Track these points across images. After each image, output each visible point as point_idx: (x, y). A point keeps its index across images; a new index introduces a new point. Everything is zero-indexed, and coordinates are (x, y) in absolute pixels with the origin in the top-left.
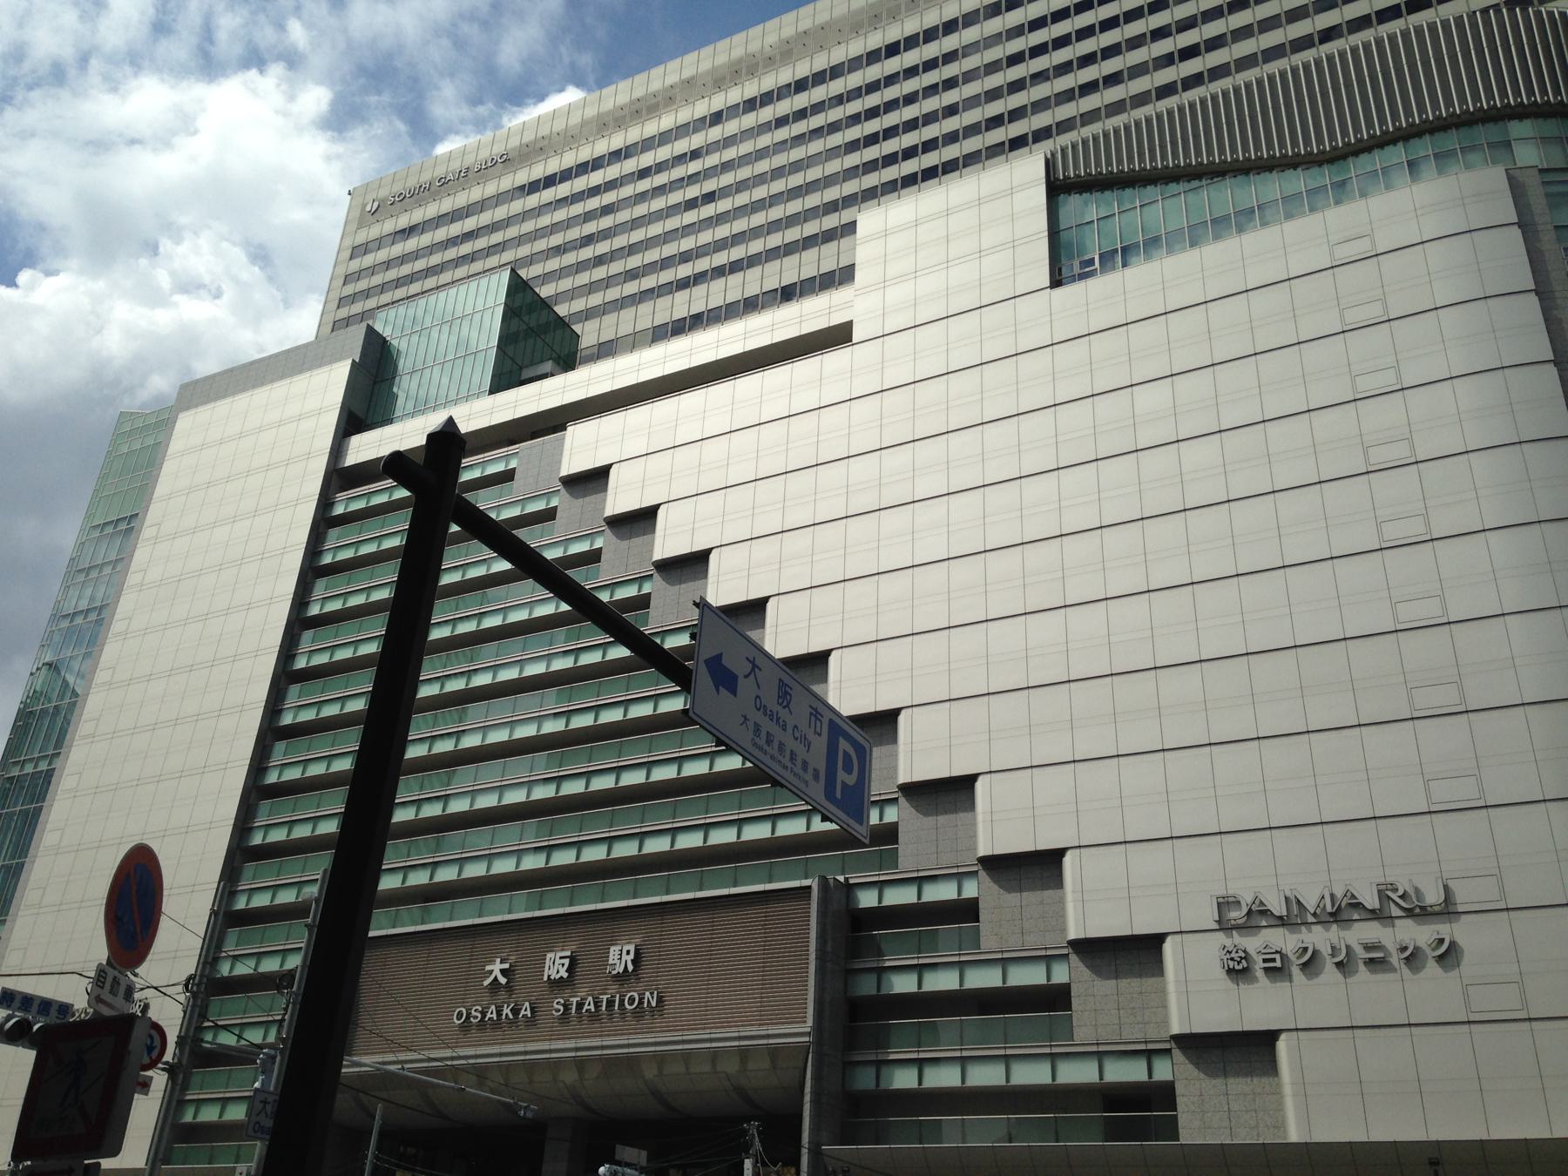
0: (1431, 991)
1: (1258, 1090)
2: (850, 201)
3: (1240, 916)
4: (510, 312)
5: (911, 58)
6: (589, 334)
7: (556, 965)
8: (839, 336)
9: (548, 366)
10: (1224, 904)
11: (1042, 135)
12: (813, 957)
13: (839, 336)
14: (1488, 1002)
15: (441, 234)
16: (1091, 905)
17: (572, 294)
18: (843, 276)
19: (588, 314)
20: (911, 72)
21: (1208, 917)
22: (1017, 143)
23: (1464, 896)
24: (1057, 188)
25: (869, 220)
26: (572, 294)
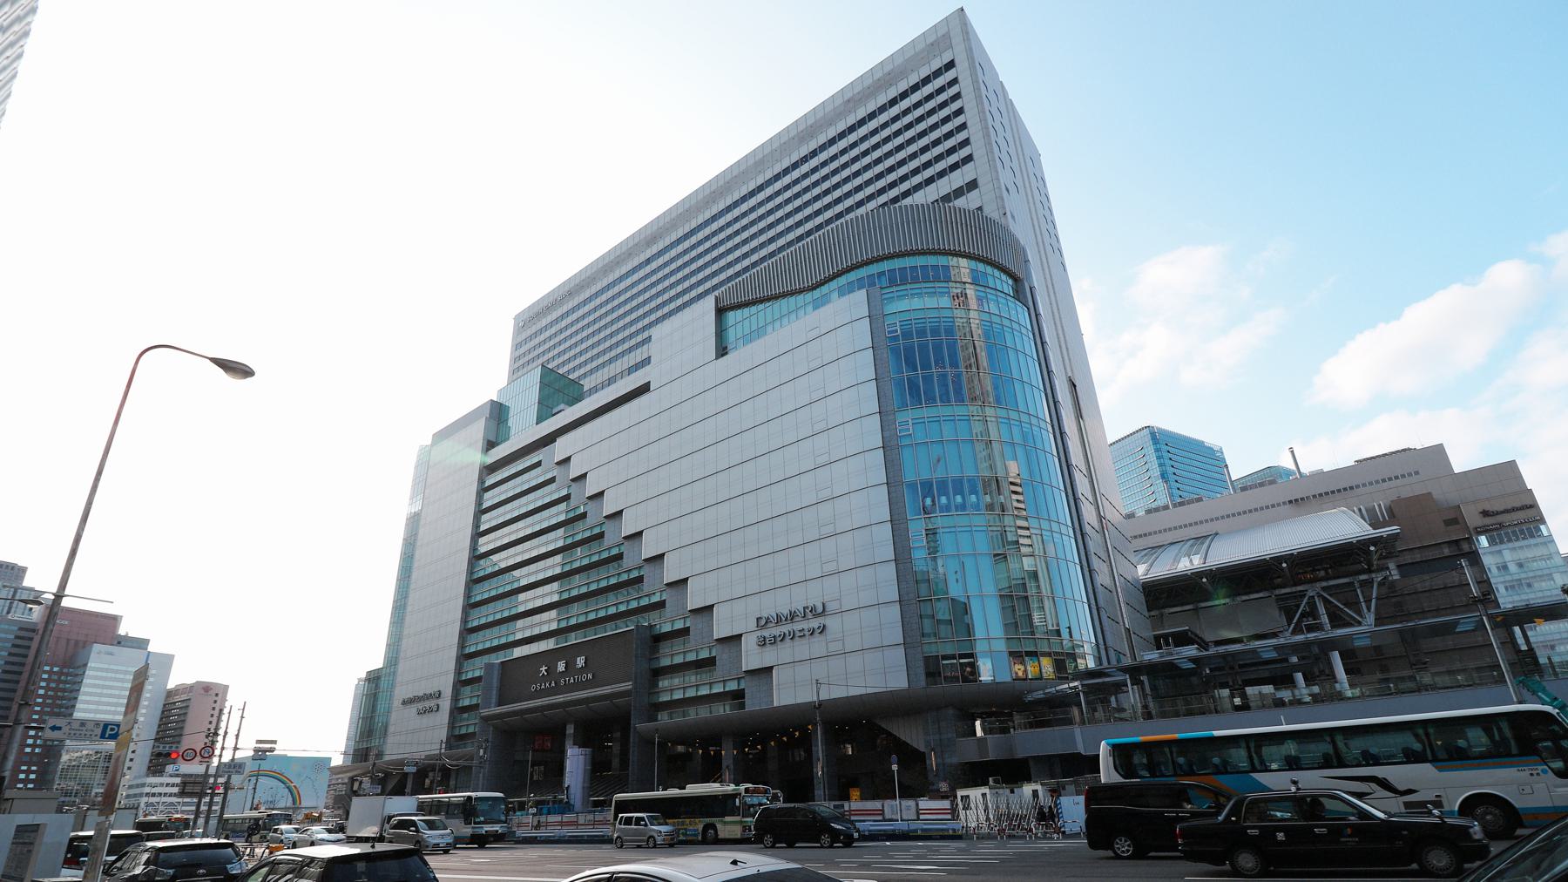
0: (817, 646)
1: (964, 435)
2: (650, 325)
3: (763, 623)
4: (544, 384)
5: (700, 235)
6: (587, 384)
7: (561, 667)
8: (644, 389)
9: (562, 406)
10: (758, 619)
11: (707, 292)
12: (607, 690)
13: (644, 389)
14: (834, 647)
15: (661, 261)
16: (722, 627)
17: (574, 370)
18: (647, 361)
19: (585, 375)
20: (824, 164)
21: (752, 625)
22: (700, 297)
23: (831, 607)
24: (721, 311)
25: (655, 332)
26: (574, 370)
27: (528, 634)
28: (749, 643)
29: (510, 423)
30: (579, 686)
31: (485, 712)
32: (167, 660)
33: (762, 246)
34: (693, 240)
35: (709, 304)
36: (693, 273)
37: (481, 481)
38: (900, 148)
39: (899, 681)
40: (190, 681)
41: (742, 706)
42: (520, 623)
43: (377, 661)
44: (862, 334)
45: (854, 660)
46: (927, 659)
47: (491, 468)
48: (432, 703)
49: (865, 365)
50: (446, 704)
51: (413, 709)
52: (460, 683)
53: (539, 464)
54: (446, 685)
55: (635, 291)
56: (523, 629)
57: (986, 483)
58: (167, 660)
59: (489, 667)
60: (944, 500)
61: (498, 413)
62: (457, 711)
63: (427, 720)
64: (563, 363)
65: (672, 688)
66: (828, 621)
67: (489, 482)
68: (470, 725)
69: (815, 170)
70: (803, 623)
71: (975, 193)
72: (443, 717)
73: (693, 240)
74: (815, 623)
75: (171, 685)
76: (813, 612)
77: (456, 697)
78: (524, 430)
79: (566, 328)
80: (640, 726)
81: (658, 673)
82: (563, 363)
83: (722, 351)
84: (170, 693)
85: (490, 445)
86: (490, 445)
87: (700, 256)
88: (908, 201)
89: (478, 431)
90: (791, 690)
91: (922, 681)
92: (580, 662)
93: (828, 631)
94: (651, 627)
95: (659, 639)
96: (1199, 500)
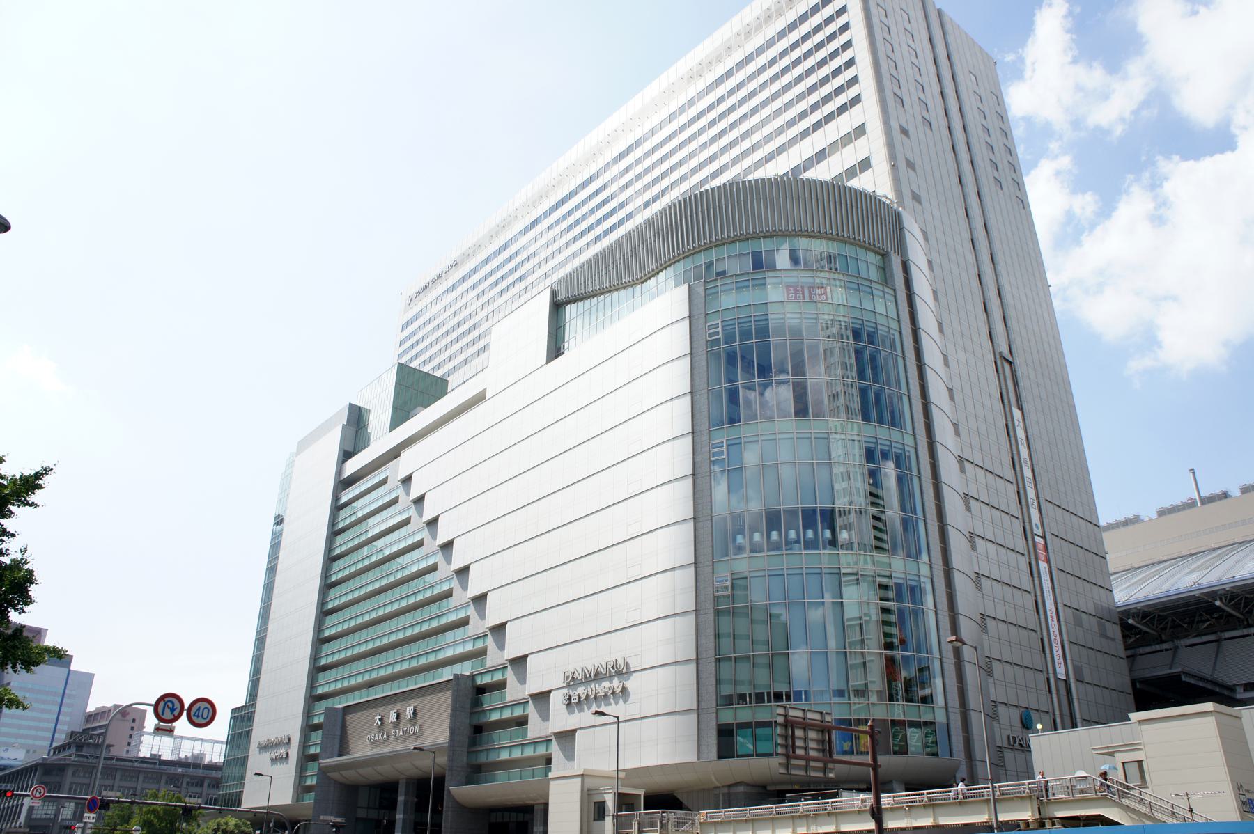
8: (479, 398)
13: (479, 398)
19: (454, 370)
20: (817, 29)
24: (557, 307)
28: (557, 700)
29: (370, 430)
31: (324, 761)
32: (87, 679)
36: (734, 143)
37: (336, 498)
38: (732, 109)
39: (687, 754)
40: (109, 704)
43: (241, 702)
44: (677, 340)
48: (282, 751)
49: (677, 378)
50: (294, 751)
51: (267, 756)
52: (309, 728)
53: (384, 481)
54: (293, 728)
57: (809, 517)
58: (87, 679)
59: (329, 712)
60: (810, 533)
62: (306, 759)
63: (280, 767)
64: (416, 356)
67: (344, 499)
69: (806, 38)
70: (599, 687)
71: (863, 140)
72: (291, 766)
75: (91, 708)
77: (305, 743)
80: (460, 792)
82: (416, 356)
83: (555, 349)
84: (91, 717)
85: (346, 455)
86: (346, 455)
87: (691, 156)
94: (473, 677)
95: (482, 690)
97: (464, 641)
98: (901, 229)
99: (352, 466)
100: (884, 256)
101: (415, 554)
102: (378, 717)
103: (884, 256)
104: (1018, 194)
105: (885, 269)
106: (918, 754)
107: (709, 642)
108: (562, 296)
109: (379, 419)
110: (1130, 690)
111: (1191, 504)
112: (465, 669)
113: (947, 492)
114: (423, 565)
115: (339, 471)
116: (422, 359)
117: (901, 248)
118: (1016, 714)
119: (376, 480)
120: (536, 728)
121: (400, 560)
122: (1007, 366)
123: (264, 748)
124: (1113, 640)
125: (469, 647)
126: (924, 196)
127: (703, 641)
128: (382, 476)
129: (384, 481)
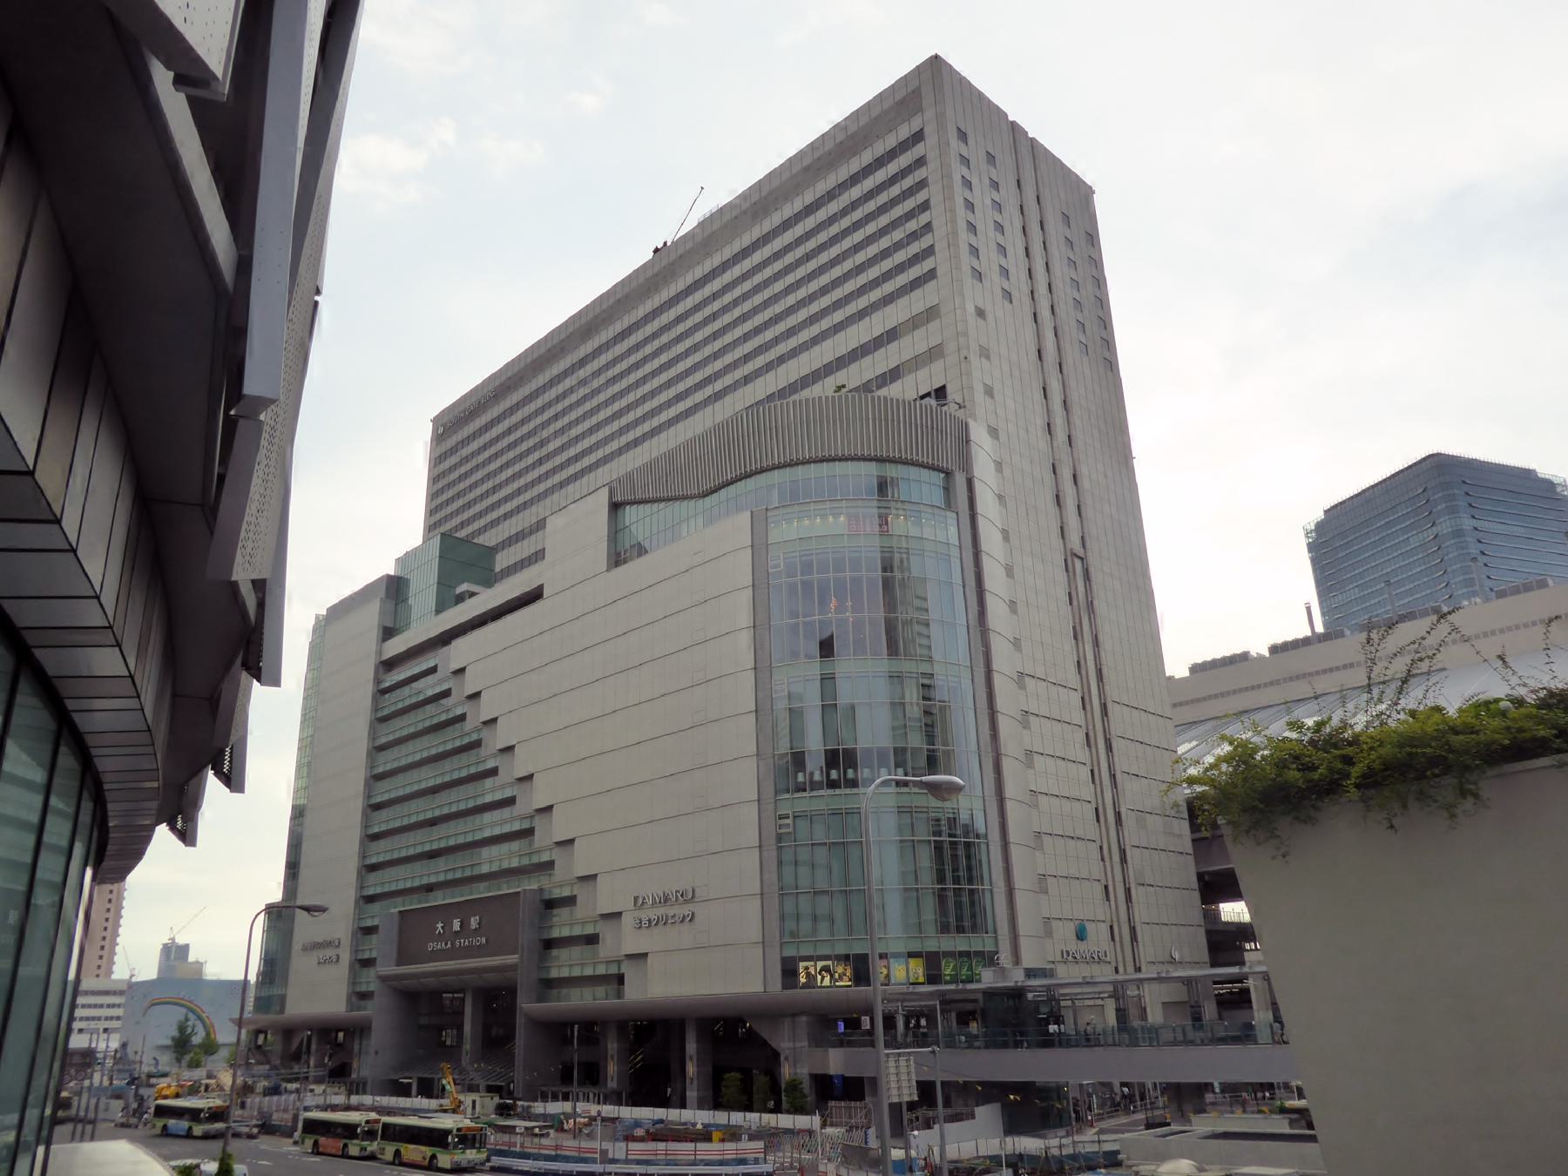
7: (456, 925)
8: (535, 596)
10: (636, 899)
13: (535, 596)
15: (737, 271)
18: (539, 556)
24: (615, 507)
27: (497, 831)
28: (628, 921)
30: (470, 952)
33: (898, 246)
34: (822, 215)
35: (603, 498)
41: (619, 995)
42: (488, 817)
43: (277, 896)
45: (706, 960)
46: (784, 960)
47: (389, 665)
48: (329, 953)
50: (346, 956)
53: (433, 670)
55: (737, 292)
56: (493, 825)
61: (394, 588)
65: (565, 964)
66: (696, 908)
68: (369, 980)
70: (675, 908)
72: (342, 971)
73: (822, 215)
74: (686, 910)
76: (687, 897)
78: (424, 623)
79: (482, 481)
80: (527, 1005)
81: (549, 944)
85: (388, 633)
86: (388, 633)
88: (806, 393)
89: (371, 617)
90: (655, 987)
91: (776, 985)
92: (474, 922)
93: (697, 919)
94: (541, 890)
95: (550, 904)
96: (1542, 584)
97: (512, 819)
98: (968, 441)
99: (396, 646)
100: (948, 474)
101: (430, 679)
102: (440, 925)
103: (948, 474)
104: (1107, 355)
105: (948, 490)
106: (1100, 739)
107: (772, 876)
108: (619, 499)
109: (423, 594)
110: (1195, 885)
111: (1305, 642)
112: (531, 884)
113: (990, 600)
114: (438, 690)
115: (380, 652)
116: (470, 529)
117: (966, 463)
118: (1070, 928)
119: (424, 667)
120: (606, 949)
121: (415, 685)
122: (1078, 563)
123: (317, 946)
124: (1180, 836)
125: (516, 826)
126: (997, 388)
127: (766, 876)
128: (431, 664)
129: (433, 670)
